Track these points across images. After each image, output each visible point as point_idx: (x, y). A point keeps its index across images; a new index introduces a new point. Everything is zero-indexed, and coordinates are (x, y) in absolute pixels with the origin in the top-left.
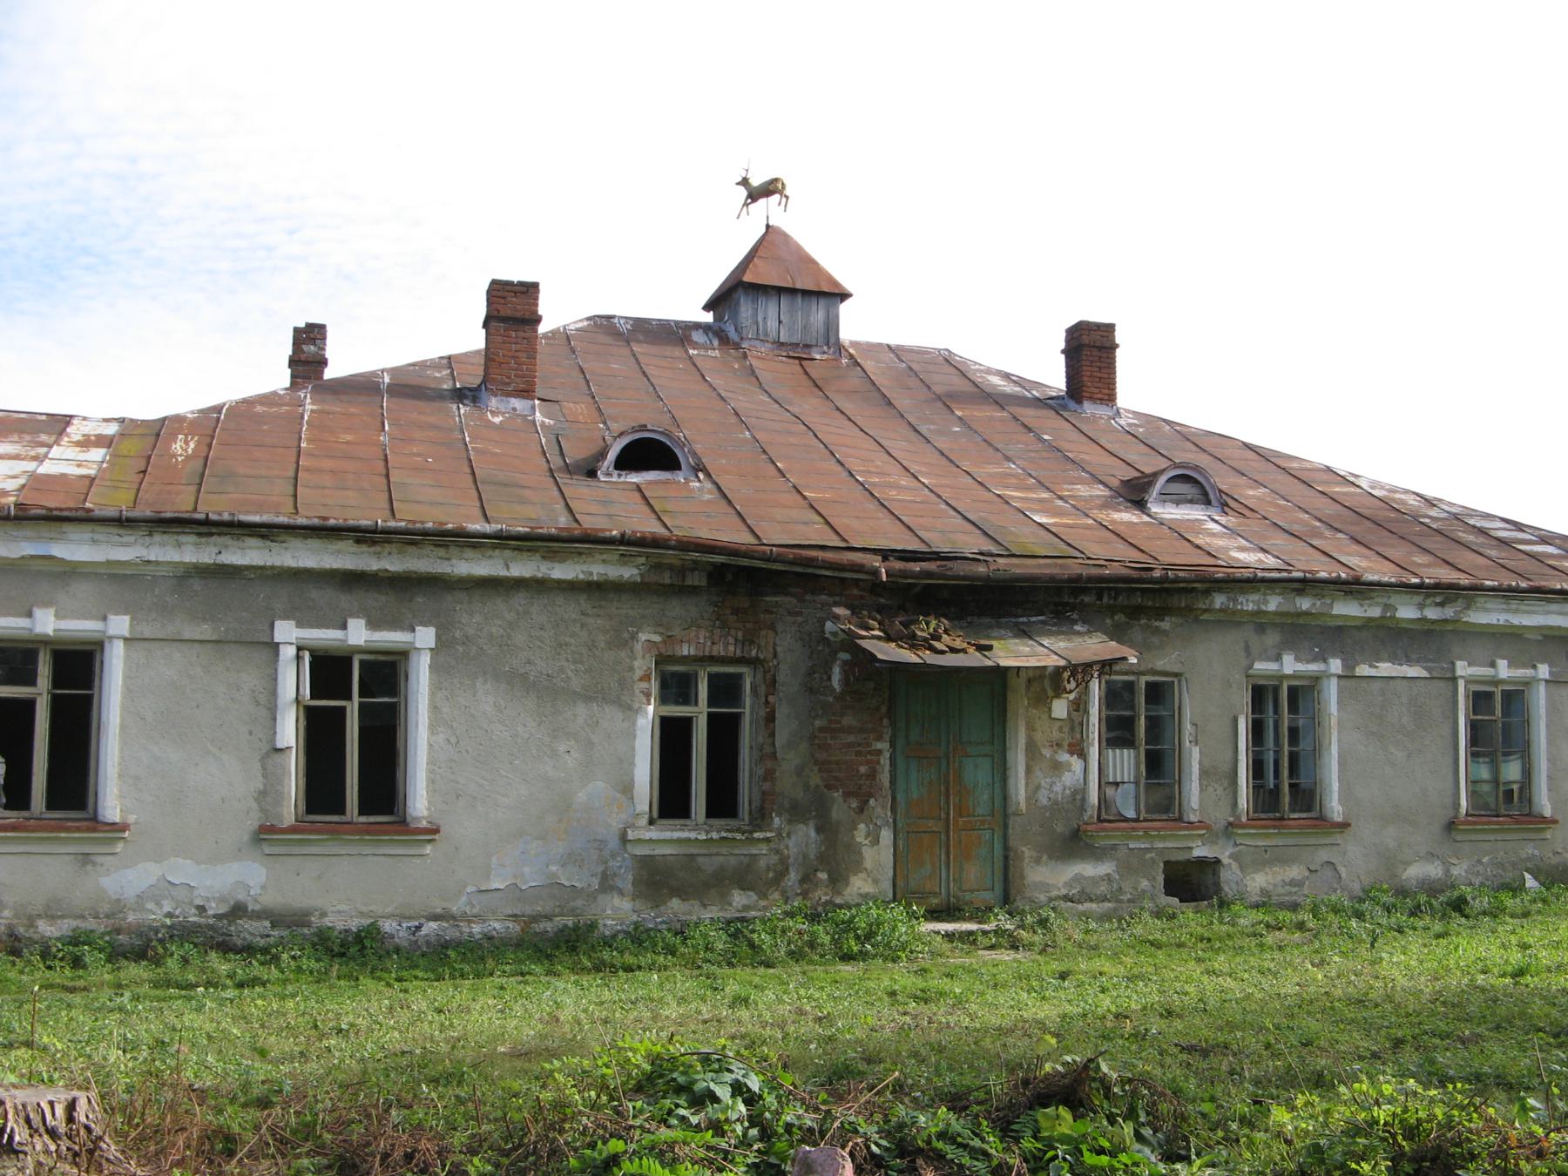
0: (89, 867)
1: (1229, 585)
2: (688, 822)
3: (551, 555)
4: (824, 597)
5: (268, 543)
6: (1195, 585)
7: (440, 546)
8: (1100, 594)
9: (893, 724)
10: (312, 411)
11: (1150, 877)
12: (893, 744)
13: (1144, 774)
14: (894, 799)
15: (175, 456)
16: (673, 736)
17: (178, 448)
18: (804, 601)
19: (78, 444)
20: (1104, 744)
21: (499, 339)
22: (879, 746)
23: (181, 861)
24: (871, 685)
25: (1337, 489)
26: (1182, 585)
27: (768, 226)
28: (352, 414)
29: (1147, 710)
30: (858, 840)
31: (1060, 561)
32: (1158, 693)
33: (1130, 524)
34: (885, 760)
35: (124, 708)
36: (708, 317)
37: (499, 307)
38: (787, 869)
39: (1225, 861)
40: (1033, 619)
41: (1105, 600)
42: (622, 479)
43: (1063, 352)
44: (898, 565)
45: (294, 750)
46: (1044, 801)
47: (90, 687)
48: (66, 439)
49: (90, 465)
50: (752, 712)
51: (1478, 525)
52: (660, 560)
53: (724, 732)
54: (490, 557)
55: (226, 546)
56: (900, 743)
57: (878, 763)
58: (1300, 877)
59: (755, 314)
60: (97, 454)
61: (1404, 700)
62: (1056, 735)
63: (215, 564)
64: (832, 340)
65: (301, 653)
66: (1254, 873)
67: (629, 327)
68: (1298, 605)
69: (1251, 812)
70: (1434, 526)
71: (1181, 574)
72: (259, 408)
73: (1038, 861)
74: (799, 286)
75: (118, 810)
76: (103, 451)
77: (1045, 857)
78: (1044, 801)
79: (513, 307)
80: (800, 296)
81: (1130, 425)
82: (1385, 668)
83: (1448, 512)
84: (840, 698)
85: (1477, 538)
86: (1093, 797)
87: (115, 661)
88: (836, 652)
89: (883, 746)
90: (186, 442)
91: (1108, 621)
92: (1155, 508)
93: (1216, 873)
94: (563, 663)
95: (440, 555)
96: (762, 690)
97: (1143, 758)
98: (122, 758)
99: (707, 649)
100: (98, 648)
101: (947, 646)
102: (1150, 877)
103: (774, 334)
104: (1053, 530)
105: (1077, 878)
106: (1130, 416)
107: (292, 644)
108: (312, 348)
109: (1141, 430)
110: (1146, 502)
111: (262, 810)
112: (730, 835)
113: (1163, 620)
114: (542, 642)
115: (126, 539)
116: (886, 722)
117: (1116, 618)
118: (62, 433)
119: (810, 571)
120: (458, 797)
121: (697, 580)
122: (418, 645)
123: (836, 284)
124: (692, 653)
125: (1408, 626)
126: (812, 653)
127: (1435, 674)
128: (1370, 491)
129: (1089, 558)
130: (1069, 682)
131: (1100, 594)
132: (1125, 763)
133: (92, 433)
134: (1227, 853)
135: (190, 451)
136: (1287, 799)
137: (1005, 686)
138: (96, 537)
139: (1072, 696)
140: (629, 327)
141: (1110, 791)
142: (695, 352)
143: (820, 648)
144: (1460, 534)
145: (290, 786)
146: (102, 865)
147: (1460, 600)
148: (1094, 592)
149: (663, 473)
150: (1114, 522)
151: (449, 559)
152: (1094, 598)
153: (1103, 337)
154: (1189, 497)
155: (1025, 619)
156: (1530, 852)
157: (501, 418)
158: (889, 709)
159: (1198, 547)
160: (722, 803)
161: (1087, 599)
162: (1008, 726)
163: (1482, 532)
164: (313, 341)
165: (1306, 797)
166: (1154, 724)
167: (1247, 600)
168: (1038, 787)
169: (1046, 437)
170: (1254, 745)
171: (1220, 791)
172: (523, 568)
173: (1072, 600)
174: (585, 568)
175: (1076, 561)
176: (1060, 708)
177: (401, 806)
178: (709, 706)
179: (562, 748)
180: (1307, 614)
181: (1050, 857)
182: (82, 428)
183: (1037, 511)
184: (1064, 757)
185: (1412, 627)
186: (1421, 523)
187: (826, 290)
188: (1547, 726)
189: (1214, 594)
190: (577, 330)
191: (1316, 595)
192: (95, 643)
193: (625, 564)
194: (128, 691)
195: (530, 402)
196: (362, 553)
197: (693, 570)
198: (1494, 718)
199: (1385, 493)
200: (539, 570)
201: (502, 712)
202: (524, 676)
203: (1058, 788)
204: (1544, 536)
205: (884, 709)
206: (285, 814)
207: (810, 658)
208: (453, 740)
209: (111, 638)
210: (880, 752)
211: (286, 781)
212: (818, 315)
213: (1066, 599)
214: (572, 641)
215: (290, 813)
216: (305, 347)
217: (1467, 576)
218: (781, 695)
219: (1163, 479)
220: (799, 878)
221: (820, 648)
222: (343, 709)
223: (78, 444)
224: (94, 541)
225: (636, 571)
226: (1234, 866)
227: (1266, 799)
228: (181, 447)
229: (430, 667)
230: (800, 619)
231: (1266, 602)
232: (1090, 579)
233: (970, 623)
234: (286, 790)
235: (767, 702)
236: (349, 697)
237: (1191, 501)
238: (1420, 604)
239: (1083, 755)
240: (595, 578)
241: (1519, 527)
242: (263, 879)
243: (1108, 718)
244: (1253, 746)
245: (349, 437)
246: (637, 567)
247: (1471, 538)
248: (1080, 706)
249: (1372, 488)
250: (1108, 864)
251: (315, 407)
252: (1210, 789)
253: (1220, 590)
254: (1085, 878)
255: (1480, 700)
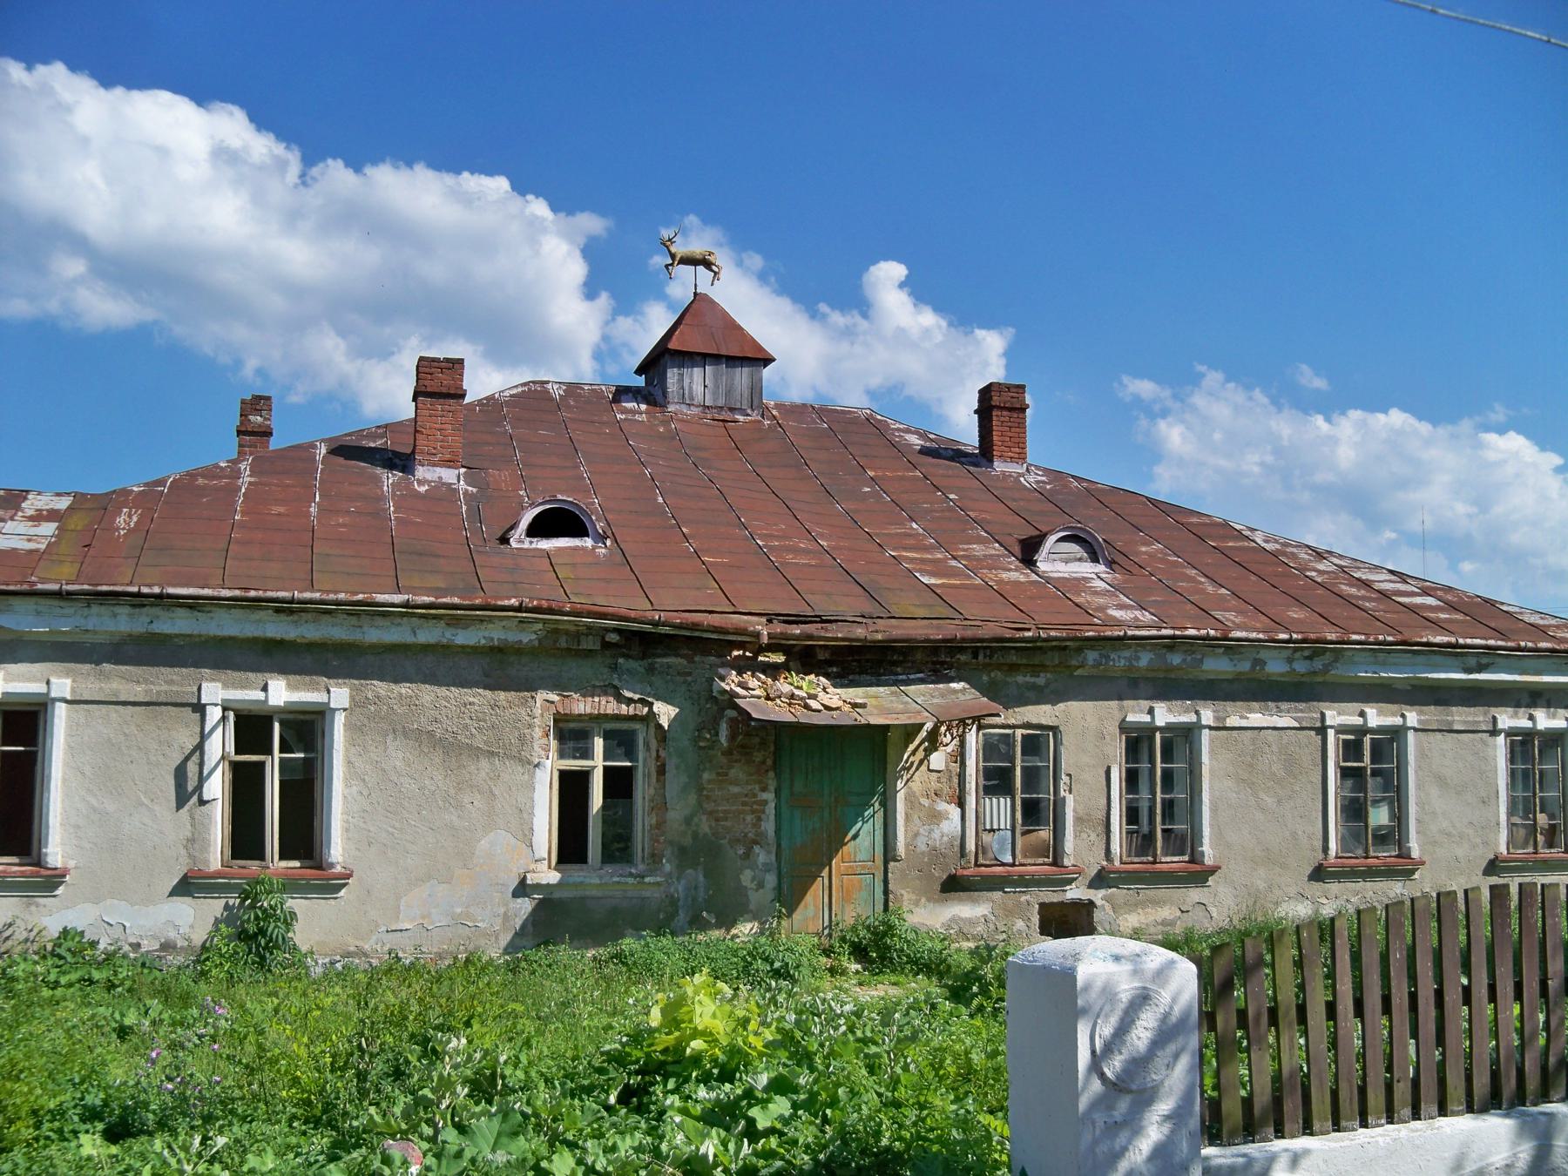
0: (33, 908)
1: (1101, 643)
2: (584, 866)
3: (454, 622)
4: (713, 658)
5: (196, 613)
6: (1068, 643)
7: (352, 614)
8: (975, 653)
9: (778, 776)
10: (250, 483)
11: (1026, 918)
12: (778, 792)
13: (1020, 821)
14: (779, 846)
15: (118, 529)
16: (572, 787)
17: (122, 521)
18: (694, 662)
19: (31, 518)
20: (981, 793)
21: (426, 413)
22: (765, 796)
23: (116, 902)
24: (757, 740)
25: (1230, 544)
26: (1054, 643)
27: (695, 294)
28: (288, 486)
29: (1023, 761)
30: (744, 884)
31: (934, 622)
32: (1033, 745)
33: (1017, 583)
34: (771, 809)
35: (66, 764)
36: (640, 381)
37: (426, 383)
38: (677, 912)
39: (1099, 902)
40: (912, 677)
41: (981, 657)
42: (534, 546)
43: (976, 412)
44: (778, 628)
45: (220, 801)
46: (923, 848)
47: (35, 745)
48: (20, 514)
49: (39, 539)
50: (644, 766)
51: (1364, 577)
52: (555, 626)
53: (619, 783)
54: (399, 624)
55: (158, 617)
56: (785, 793)
57: (764, 812)
58: (1172, 917)
59: (681, 380)
60: (49, 528)
61: (1274, 748)
62: (934, 785)
63: (147, 633)
64: (756, 403)
65: (226, 714)
66: (1126, 913)
67: (562, 393)
68: (1169, 661)
69: (1124, 855)
70: (1319, 580)
71: (1053, 633)
72: (200, 481)
73: (917, 903)
74: (724, 352)
75: (60, 856)
76: (55, 525)
77: (923, 900)
78: (923, 848)
79: (441, 381)
80: (724, 360)
81: (1038, 482)
82: (1256, 718)
83: (1335, 565)
84: (728, 752)
85: (1359, 590)
86: (971, 845)
87: (56, 721)
88: (723, 710)
89: (769, 796)
90: (130, 516)
91: (985, 678)
92: (1042, 566)
93: (1090, 915)
94: (468, 721)
95: (352, 623)
96: (654, 744)
97: (1019, 808)
98: (64, 808)
99: (602, 708)
100: (42, 708)
101: (822, 705)
102: (1026, 918)
103: (701, 397)
104: (938, 591)
105: (954, 919)
106: (1040, 473)
107: (216, 705)
108: (259, 418)
109: (1048, 487)
110: (1036, 561)
111: (190, 856)
112: (623, 880)
113: (1038, 676)
114: (448, 702)
115: (66, 611)
116: (771, 774)
117: (993, 675)
118: (18, 508)
119: (697, 634)
120: (370, 844)
121: (590, 644)
122: (332, 706)
123: (760, 349)
124: (588, 710)
125: (1279, 679)
126: (700, 710)
127: (1305, 724)
128: (1263, 545)
129: (966, 619)
130: (945, 736)
131: (975, 653)
132: (1001, 811)
133: (44, 508)
134: (1100, 896)
135: (132, 525)
136: (1159, 844)
137: (885, 739)
138: (40, 608)
139: (949, 749)
140: (562, 393)
141: (986, 838)
142: (623, 417)
143: (708, 706)
144: (1343, 587)
145: (216, 834)
146: (45, 906)
147: (1328, 653)
148: (970, 651)
149: (572, 539)
150: (1000, 582)
151: (361, 627)
152: (970, 656)
153: (1012, 397)
154: (1078, 556)
155: (904, 677)
156: (1398, 892)
157: (427, 487)
158: (774, 762)
159: (1077, 605)
160: (618, 848)
161: (963, 658)
162: (888, 776)
163: (1366, 584)
164: (258, 411)
165: (1186, 843)
166: (1031, 776)
167: (1119, 657)
168: (916, 835)
169: (952, 496)
170: (1128, 792)
171: (1093, 837)
172: (428, 635)
173: (948, 660)
174: (481, 634)
175: (952, 622)
176: (938, 760)
177: (318, 851)
178: (605, 759)
179: (466, 800)
180: (1179, 668)
181: (929, 900)
182: (36, 503)
183: (924, 572)
184: (942, 806)
185: (1282, 679)
186: (1307, 577)
187: (749, 356)
188: (1416, 772)
189: (1086, 651)
190: (511, 396)
191: (1186, 651)
192: (41, 700)
193: (523, 630)
194: (70, 748)
195: (456, 472)
196: (281, 621)
197: (587, 635)
198: (1362, 765)
199: (1278, 547)
200: (443, 636)
201: (409, 766)
202: (431, 734)
203: (936, 835)
204: (1428, 587)
205: (769, 762)
206: (212, 860)
207: (699, 714)
208: (365, 793)
209: (55, 700)
210: (765, 802)
211: (213, 829)
212: (742, 376)
213: (943, 658)
214: (476, 700)
215: (216, 859)
216: (251, 418)
217: (1338, 629)
218: (671, 749)
219: (1052, 539)
220: (688, 919)
221: (708, 706)
222: (262, 764)
223: (31, 518)
224: (38, 613)
225: (534, 637)
226: (1108, 906)
227: (1142, 843)
228: (125, 521)
229: (345, 725)
230: (689, 679)
231: (1138, 659)
232: (963, 640)
233: (851, 681)
234: (212, 837)
235: (658, 757)
236: (268, 751)
237: (1080, 560)
238: (1289, 658)
239: (961, 804)
240: (496, 643)
241: (1402, 577)
242: (191, 920)
243: (985, 767)
244: (1127, 793)
245: (281, 510)
246: (535, 633)
247: (1353, 591)
248: (960, 756)
249: (1266, 541)
250: (986, 906)
251: (253, 480)
252: (1084, 836)
253: (1092, 648)
254: (962, 919)
255: (1351, 749)
